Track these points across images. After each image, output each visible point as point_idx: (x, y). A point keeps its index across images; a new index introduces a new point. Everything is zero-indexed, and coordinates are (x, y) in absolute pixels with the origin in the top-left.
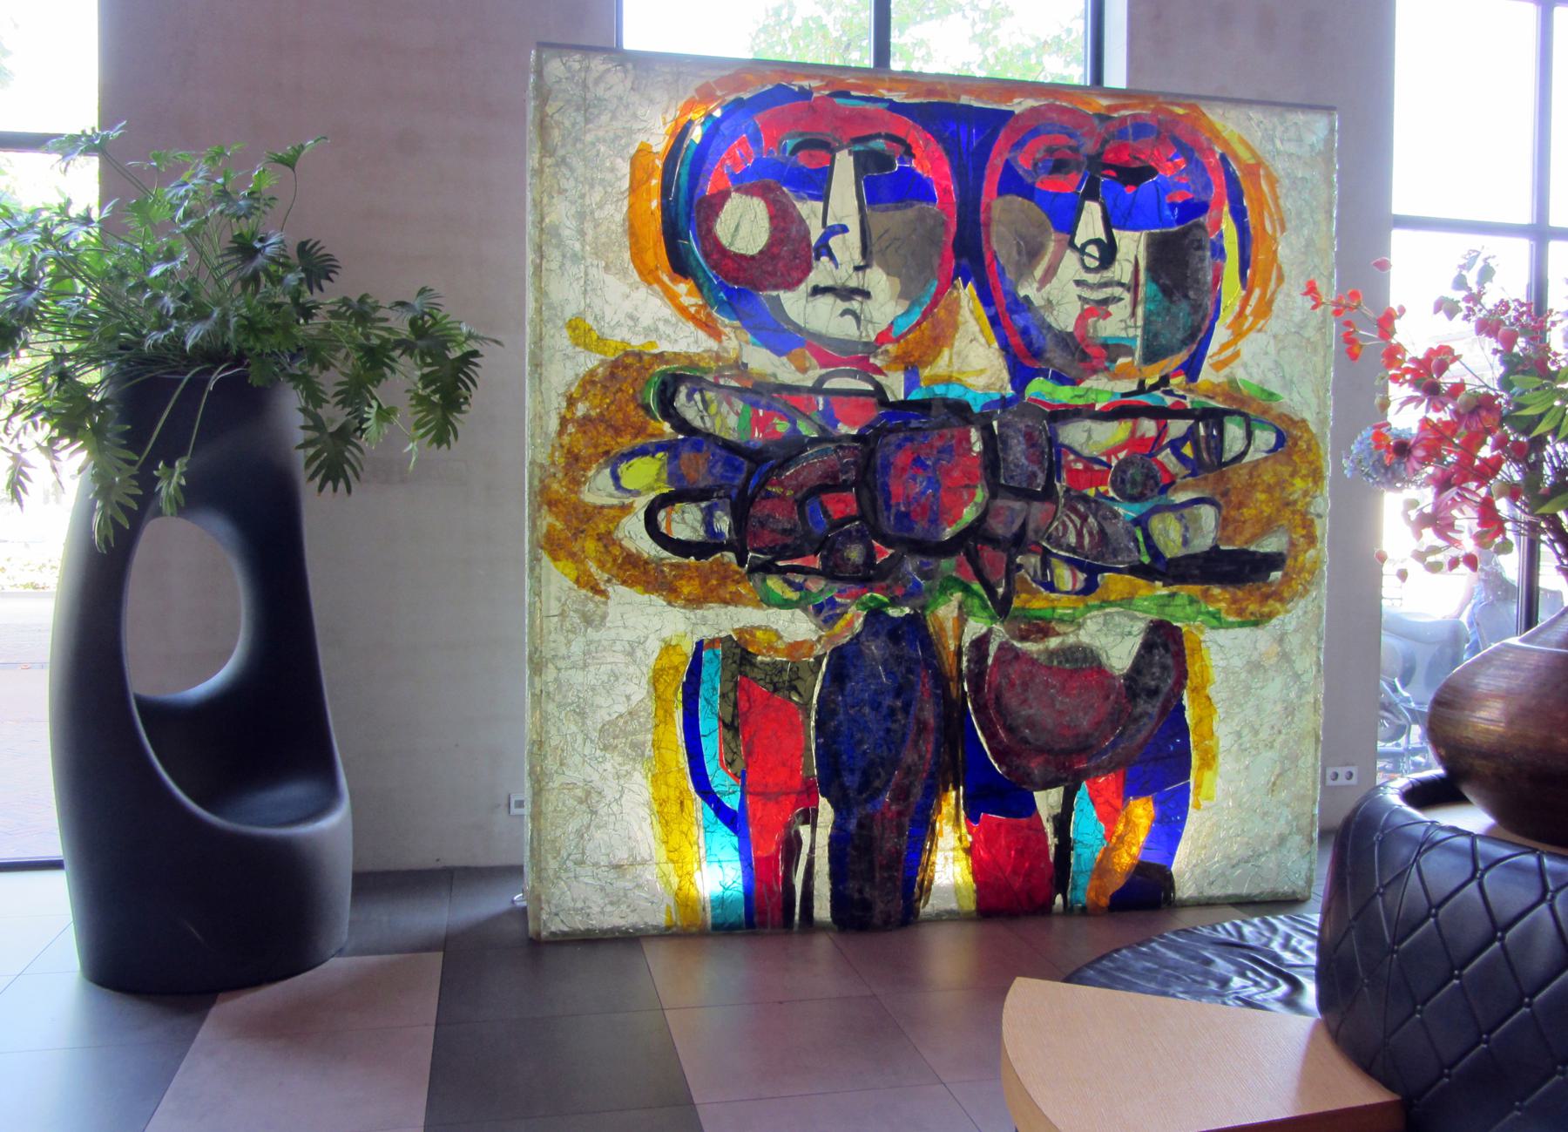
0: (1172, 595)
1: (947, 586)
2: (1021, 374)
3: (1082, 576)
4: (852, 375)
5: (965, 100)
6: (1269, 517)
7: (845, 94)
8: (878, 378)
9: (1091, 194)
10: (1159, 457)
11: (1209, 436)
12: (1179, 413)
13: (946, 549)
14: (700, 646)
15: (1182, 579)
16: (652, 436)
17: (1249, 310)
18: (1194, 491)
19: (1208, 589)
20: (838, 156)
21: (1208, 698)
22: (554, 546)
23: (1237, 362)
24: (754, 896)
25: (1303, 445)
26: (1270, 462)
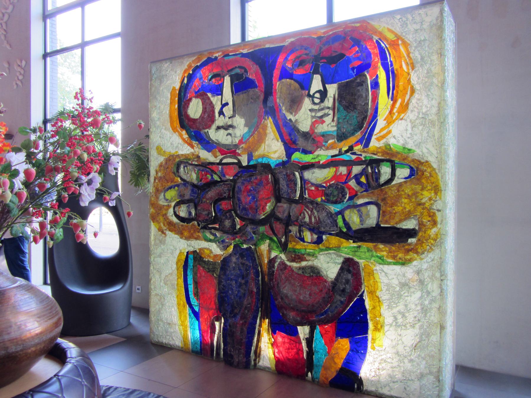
0: (359, 247)
1: (263, 237)
2: (289, 150)
3: (315, 236)
4: (230, 157)
5: (267, 46)
6: (409, 211)
7: (228, 55)
8: (239, 157)
9: (316, 72)
10: (349, 183)
11: (373, 172)
12: (358, 162)
13: (262, 222)
14: (188, 253)
15: (362, 240)
16: (176, 182)
17: (395, 110)
18: (368, 199)
19: (376, 246)
20: (225, 78)
21: (378, 297)
22: (154, 218)
23: (390, 135)
24: (202, 342)
25: (427, 174)
26: (408, 184)
